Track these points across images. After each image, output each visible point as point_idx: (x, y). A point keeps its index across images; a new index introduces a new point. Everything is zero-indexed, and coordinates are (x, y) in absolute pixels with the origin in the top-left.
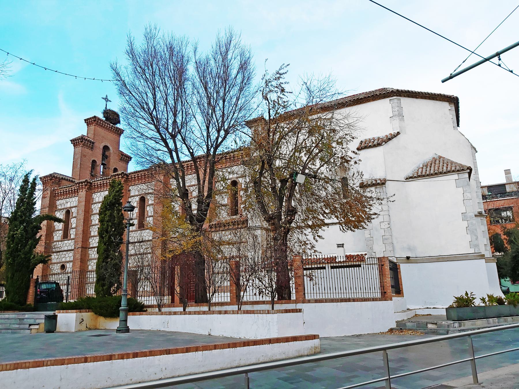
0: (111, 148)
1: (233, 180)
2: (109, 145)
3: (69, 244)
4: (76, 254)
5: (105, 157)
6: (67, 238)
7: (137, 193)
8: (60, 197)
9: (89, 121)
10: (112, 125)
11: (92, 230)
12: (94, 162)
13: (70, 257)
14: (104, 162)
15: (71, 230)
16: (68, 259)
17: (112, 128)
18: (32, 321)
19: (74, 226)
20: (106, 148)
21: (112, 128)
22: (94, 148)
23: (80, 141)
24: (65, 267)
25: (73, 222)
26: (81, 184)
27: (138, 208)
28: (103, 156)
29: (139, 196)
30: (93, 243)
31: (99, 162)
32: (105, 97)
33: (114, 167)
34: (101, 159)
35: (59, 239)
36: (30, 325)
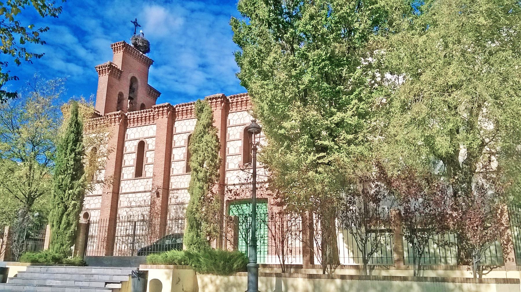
0: (139, 80)
1: (140, 140)
2: (137, 76)
3: (142, 184)
4: (105, 200)
5: (132, 90)
6: (141, 175)
7: (184, 130)
8: (241, 108)
9: (119, 46)
10: (142, 53)
11: (125, 172)
12: (121, 95)
13: (95, 204)
14: (131, 96)
15: (146, 166)
16: (93, 206)
17: (141, 57)
18: (107, 279)
19: (150, 161)
20: (133, 80)
21: (141, 57)
22: (122, 79)
23: (107, 68)
24: (89, 215)
25: (149, 156)
26: (156, 109)
27: (137, 153)
28: (130, 88)
29: (187, 134)
30: (126, 188)
31: (126, 95)
32: (134, 20)
33: (141, 103)
34: (128, 92)
35: (181, 172)
36: (106, 283)
